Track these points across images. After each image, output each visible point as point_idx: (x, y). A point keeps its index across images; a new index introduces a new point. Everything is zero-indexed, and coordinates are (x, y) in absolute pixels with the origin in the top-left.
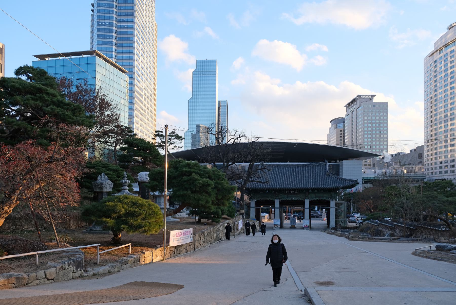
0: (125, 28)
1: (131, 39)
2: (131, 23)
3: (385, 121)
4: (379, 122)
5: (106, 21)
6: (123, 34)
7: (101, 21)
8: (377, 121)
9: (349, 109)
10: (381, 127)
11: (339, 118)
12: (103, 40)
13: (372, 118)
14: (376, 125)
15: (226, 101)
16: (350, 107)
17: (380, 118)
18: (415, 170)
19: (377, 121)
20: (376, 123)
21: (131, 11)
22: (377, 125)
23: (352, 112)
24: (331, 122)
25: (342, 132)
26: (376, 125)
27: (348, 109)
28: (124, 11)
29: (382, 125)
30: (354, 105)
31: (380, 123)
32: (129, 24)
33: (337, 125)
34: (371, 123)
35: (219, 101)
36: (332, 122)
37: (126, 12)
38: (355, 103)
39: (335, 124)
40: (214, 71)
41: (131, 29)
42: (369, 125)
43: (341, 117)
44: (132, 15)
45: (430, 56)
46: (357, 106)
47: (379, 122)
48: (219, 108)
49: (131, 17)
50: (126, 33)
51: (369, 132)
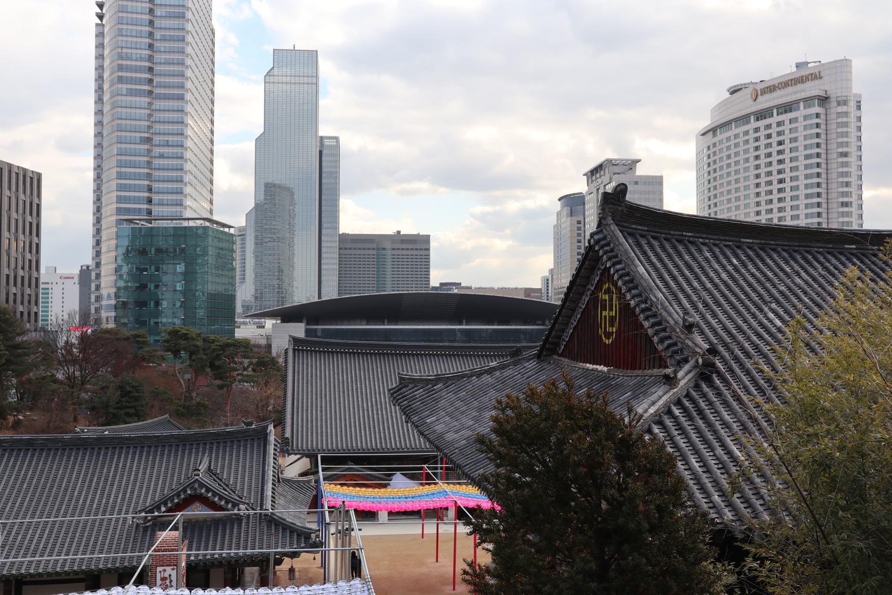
2: (178, 183)
9: (592, 181)
11: (577, 194)
12: (129, 86)
16: (594, 178)
24: (560, 200)
27: (590, 180)
35: (322, 138)
36: (563, 201)
38: (602, 172)
39: (567, 205)
41: (179, 195)
43: (579, 193)
48: (321, 152)
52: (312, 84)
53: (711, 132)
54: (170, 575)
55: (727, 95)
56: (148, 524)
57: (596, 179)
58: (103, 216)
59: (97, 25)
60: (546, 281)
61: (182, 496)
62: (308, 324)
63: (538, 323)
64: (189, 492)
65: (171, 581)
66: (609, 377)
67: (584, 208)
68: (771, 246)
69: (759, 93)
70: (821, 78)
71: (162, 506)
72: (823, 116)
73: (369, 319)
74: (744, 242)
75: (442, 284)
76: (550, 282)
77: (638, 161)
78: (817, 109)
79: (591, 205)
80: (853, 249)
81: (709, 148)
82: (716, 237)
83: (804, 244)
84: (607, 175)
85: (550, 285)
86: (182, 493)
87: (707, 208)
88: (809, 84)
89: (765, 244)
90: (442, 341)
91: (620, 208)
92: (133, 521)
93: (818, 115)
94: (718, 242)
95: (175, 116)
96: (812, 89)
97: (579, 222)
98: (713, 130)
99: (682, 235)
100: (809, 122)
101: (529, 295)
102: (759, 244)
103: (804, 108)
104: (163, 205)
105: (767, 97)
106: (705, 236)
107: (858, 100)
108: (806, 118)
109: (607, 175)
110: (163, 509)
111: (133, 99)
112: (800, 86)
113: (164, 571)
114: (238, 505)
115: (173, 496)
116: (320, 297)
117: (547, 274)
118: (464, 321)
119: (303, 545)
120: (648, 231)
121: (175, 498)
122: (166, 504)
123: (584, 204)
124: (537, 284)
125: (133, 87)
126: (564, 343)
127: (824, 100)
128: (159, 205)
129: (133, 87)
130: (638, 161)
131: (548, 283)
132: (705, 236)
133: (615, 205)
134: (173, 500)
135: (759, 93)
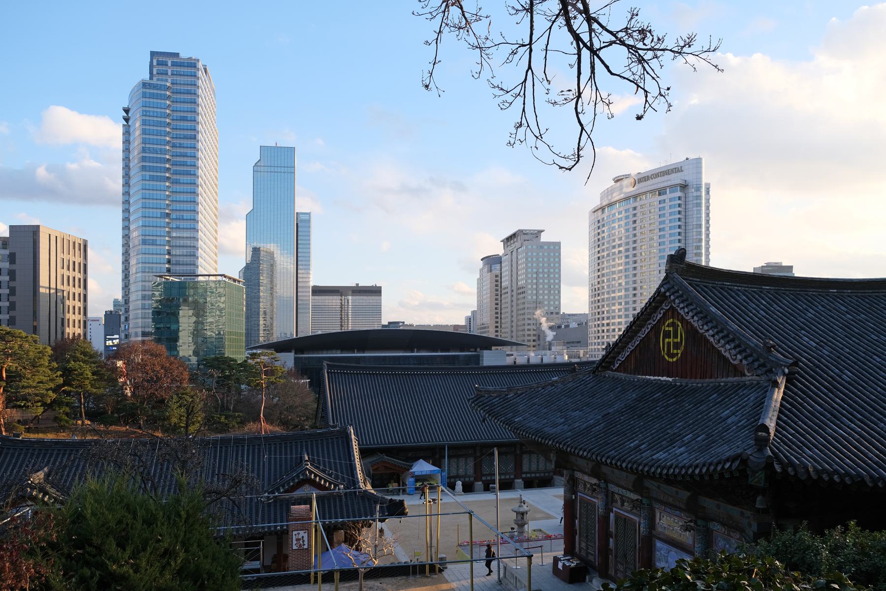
0: (184, 156)
1: (192, 173)
3: (557, 270)
4: (549, 272)
5: (155, 146)
6: (180, 165)
7: (147, 146)
8: (546, 270)
9: (507, 246)
10: (551, 278)
12: (152, 173)
13: (538, 265)
14: (544, 276)
15: (309, 214)
16: (509, 243)
17: (549, 265)
18: (579, 354)
19: (546, 270)
20: (543, 272)
21: (193, 133)
22: (546, 276)
23: (512, 252)
24: (482, 260)
25: (499, 279)
26: (544, 276)
27: (506, 245)
28: (182, 132)
29: (552, 276)
30: (514, 242)
31: (549, 273)
32: (189, 151)
33: (491, 267)
34: (536, 273)
35: (297, 213)
37: (186, 133)
38: (515, 240)
40: (291, 167)
42: (535, 276)
44: (194, 138)
45: (594, 212)
46: (518, 244)
47: (549, 272)
48: (297, 224)
49: (193, 140)
50: (184, 164)
51: (535, 286)
52: (291, 173)
53: (601, 210)
54: (303, 537)
55: (613, 183)
56: (270, 501)
57: (511, 244)
58: (131, 274)
59: (124, 125)
60: (469, 320)
61: (296, 481)
62: (296, 353)
63: (471, 350)
64: (301, 477)
65: (303, 541)
66: (676, 385)
67: (501, 266)
68: (782, 291)
69: (637, 182)
70: (682, 171)
71: (281, 488)
72: (683, 199)
73: (343, 349)
74: (764, 289)
75: (390, 323)
76: (472, 320)
77: (542, 231)
78: (679, 194)
79: (507, 263)
80: (835, 292)
81: (599, 222)
82: (746, 285)
83: (803, 289)
84: (519, 242)
85: (472, 322)
86: (296, 478)
87: (597, 265)
88: (673, 175)
89: (778, 290)
90: (424, 364)
91: (682, 266)
92: (257, 500)
93: (680, 198)
94: (747, 289)
95: (188, 197)
96: (676, 179)
97: (497, 276)
98: (602, 209)
99: (723, 284)
100: (673, 203)
101: (457, 330)
102: (774, 290)
103: (670, 193)
104: (179, 264)
105: (642, 184)
106: (738, 285)
107: (708, 187)
108: (671, 200)
109: (519, 242)
110: (282, 490)
111: (155, 183)
112: (666, 177)
113: (299, 534)
114: (338, 486)
115: (289, 480)
116: (297, 335)
117: (470, 314)
118: (415, 350)
119: (386, 514)
120: (700, 282)
121: (291, 481)
122: (283, 486)
123: (501, 262)
124: (462, 322)
125: (155, 174)
126: (619, 362)
127: (684, 187)
128: (176, 264)
129: (155, 174)
130: (542, 231)
131: (470, 321)
132: (738, 285)
133: (678, 263)
134: (289, 483)
135: (637, 182)
